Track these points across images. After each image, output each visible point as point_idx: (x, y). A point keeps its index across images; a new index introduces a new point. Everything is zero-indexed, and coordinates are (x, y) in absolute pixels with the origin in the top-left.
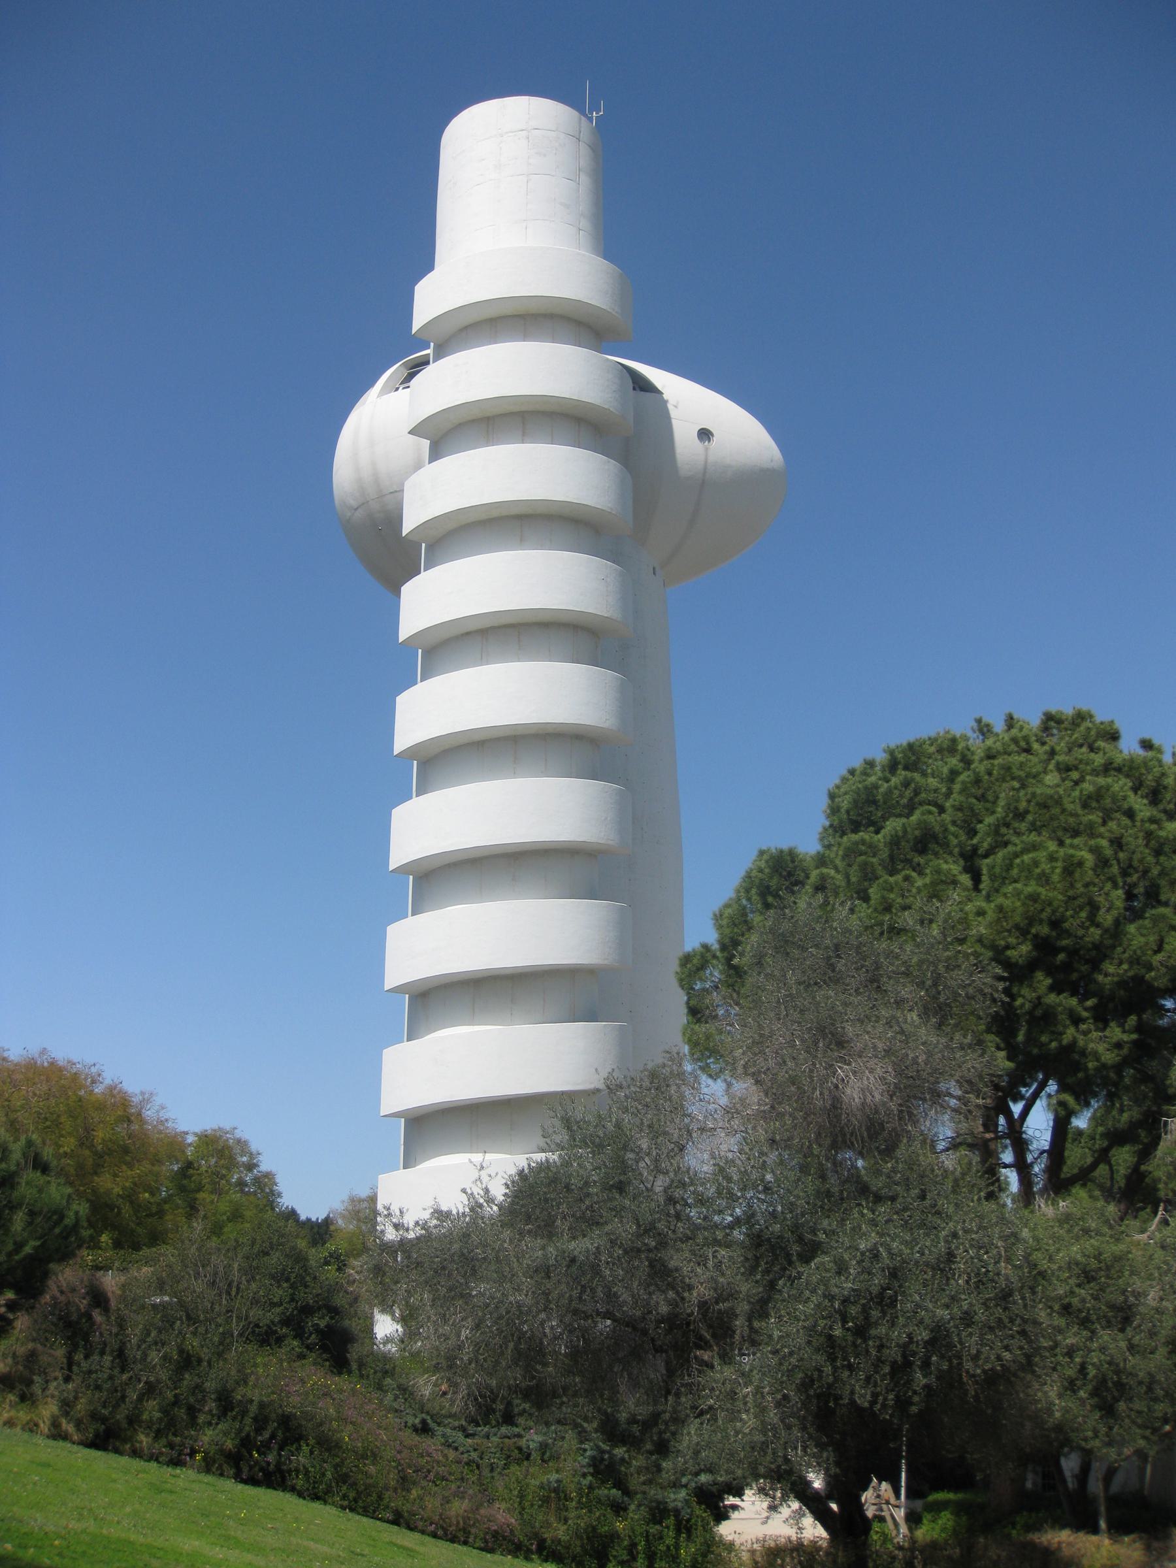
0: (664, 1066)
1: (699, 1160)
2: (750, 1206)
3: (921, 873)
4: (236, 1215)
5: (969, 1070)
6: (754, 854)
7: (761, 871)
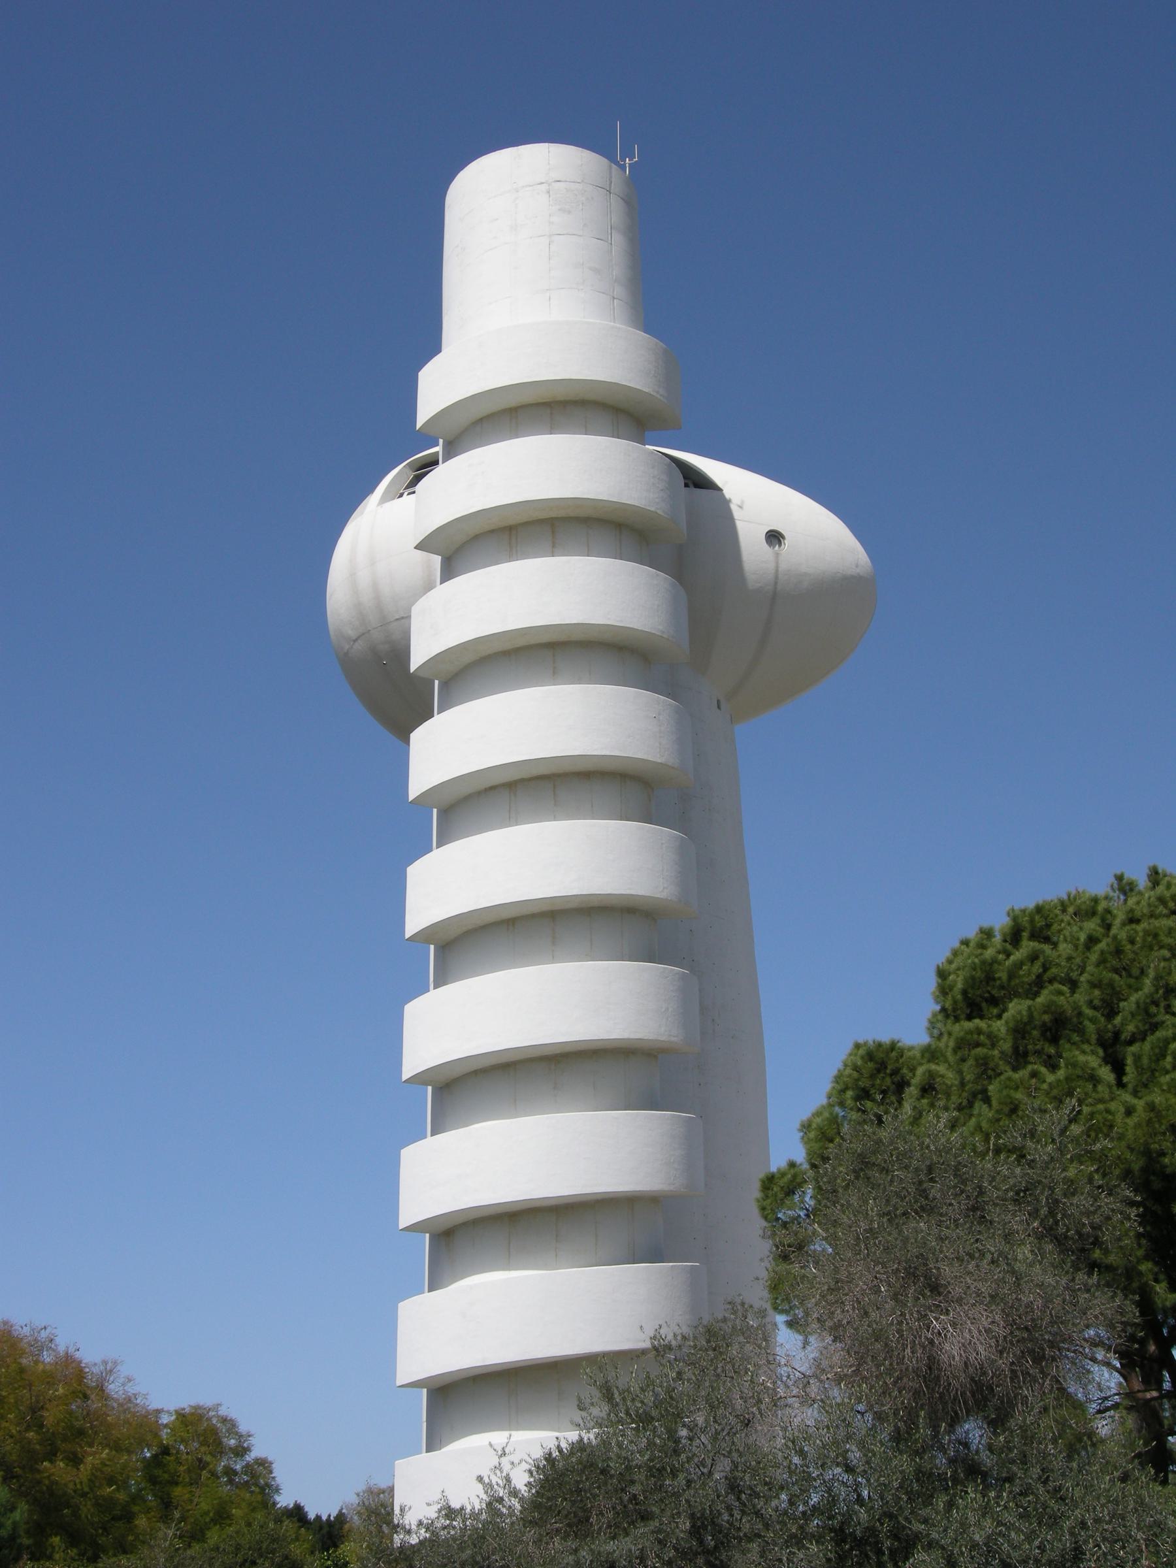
0: (725, 1320)
1: (770, 1439)
2: (829, 1491)
3: (1053, 1068)
4: (221, 1516)
5: (1096, 1317)
6: (848, 1047)
7: (856, 1068)
